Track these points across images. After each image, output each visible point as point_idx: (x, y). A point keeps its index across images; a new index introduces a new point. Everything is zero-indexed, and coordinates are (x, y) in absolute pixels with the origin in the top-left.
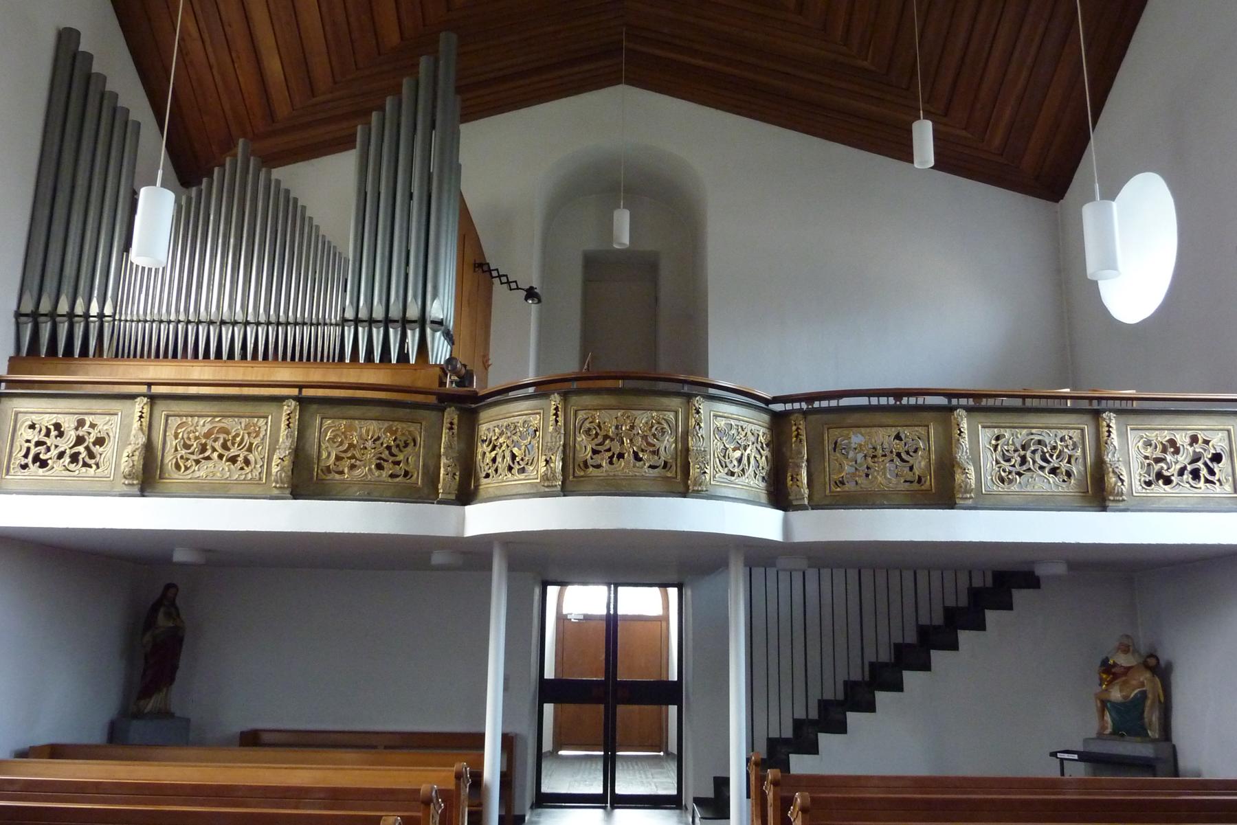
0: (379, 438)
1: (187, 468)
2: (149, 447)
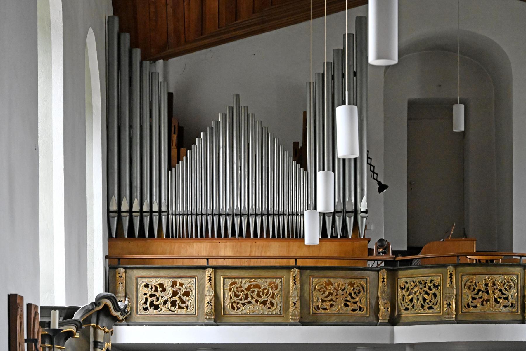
0: (345, 289)
1: (238, 309)
2: (216, 296)
